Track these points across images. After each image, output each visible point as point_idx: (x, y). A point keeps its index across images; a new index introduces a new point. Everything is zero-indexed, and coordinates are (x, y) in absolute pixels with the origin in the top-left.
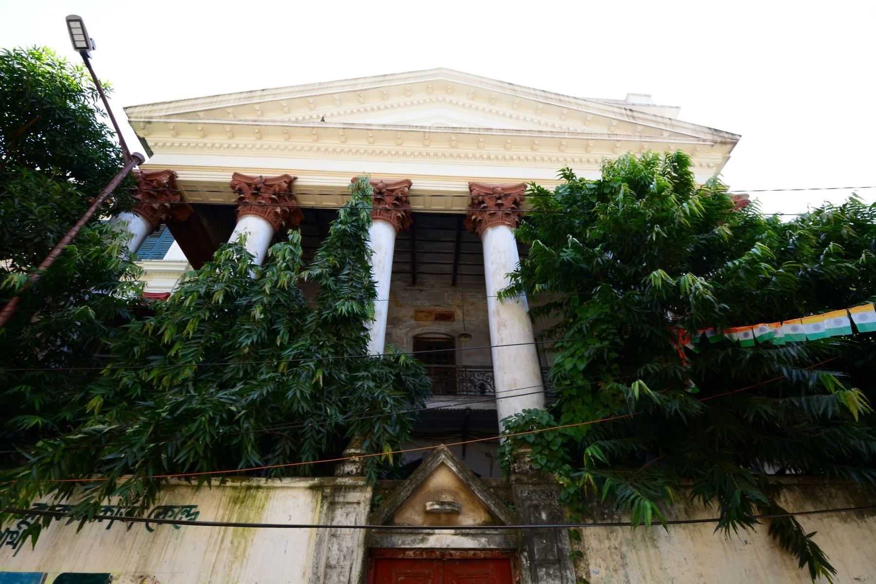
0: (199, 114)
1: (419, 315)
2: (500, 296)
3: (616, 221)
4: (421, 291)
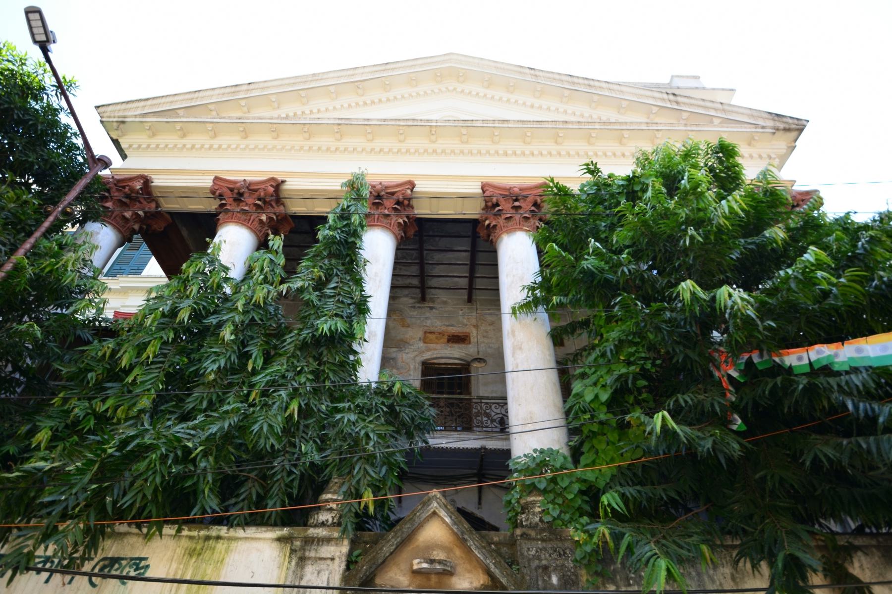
0: (179, 111)
1: (428, 336)
2: (514, 311)
3: (645, 223)
4: (431, 308)
